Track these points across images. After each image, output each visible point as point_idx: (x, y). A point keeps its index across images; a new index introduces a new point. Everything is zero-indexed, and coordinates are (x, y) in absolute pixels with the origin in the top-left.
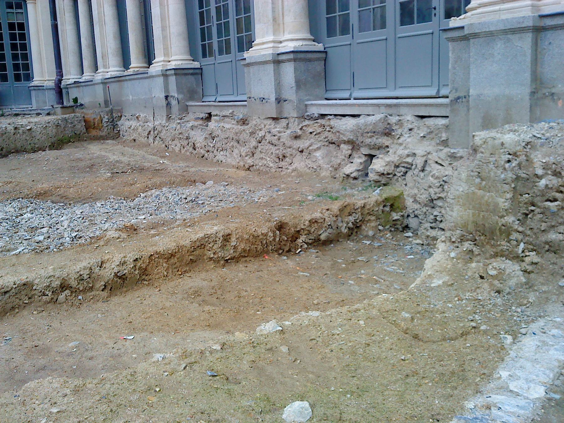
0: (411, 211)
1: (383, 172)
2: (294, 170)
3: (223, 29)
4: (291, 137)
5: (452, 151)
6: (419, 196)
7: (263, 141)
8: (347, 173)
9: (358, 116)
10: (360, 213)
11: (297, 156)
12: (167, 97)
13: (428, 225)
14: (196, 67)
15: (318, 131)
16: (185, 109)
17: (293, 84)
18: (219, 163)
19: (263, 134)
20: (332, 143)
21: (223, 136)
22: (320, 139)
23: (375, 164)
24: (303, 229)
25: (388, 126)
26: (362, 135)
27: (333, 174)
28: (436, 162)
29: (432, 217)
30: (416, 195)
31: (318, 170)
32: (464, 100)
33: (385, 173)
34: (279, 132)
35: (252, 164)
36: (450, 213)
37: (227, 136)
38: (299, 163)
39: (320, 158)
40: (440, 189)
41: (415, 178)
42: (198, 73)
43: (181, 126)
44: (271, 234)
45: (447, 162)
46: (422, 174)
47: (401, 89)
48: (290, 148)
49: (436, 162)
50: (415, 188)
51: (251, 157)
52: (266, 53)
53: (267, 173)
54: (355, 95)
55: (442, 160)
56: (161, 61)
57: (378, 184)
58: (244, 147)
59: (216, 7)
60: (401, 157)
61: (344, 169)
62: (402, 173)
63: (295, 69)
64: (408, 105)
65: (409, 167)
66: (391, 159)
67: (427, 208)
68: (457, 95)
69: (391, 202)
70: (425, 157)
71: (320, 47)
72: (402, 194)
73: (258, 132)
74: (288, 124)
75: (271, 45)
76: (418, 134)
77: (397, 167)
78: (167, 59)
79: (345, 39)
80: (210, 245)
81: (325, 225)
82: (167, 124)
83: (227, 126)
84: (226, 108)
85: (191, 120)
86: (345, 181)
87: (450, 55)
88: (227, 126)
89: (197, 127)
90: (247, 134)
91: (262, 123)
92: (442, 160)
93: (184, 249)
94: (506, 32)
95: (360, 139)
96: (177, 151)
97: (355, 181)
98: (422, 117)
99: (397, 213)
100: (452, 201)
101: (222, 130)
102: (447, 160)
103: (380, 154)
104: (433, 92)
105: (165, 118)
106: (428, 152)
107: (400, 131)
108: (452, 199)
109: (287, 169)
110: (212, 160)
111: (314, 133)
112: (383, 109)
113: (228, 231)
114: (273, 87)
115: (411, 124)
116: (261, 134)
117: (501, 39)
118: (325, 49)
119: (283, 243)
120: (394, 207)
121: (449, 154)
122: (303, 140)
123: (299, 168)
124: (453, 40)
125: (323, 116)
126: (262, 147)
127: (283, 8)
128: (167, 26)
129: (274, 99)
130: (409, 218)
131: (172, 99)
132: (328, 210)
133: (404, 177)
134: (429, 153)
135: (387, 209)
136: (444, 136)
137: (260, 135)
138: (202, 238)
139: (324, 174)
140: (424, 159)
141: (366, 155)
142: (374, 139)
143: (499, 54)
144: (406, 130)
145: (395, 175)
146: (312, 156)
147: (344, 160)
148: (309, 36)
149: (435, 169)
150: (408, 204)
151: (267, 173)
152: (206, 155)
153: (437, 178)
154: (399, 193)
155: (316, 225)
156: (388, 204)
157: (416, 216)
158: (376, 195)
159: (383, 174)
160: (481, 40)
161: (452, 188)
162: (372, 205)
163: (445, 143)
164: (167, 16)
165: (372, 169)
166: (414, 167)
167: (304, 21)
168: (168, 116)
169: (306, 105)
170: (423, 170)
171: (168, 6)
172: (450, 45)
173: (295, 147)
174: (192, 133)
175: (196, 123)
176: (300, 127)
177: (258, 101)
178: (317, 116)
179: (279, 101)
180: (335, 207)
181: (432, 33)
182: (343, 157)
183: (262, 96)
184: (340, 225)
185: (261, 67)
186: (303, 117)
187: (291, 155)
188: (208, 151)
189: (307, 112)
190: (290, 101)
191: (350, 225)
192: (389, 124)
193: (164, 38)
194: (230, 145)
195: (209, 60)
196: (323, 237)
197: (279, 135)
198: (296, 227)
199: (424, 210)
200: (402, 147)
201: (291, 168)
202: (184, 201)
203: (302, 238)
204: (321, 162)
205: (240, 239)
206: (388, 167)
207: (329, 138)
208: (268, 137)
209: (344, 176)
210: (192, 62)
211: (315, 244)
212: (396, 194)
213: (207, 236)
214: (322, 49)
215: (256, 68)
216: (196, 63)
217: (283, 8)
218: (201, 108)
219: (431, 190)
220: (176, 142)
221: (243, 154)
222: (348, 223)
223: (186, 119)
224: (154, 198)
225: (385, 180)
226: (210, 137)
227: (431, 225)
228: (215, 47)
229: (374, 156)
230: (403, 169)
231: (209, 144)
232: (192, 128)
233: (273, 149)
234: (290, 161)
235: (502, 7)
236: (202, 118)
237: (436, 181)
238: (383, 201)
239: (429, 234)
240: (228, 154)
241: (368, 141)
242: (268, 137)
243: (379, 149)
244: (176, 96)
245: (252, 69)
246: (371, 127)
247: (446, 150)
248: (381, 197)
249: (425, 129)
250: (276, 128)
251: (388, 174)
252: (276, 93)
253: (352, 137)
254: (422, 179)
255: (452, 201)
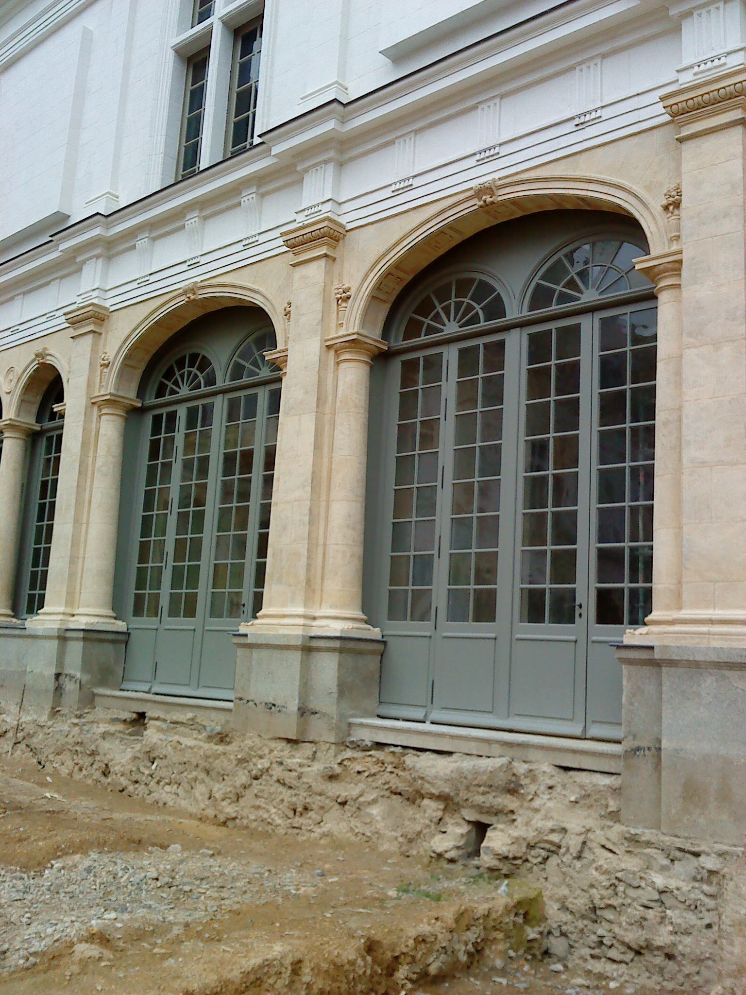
0: (555, 926)
1: (506, 854)
2: (324, 835)
3: (186, 577)
4: (323, 777)
5: (633, 831)
6: (570, 900)
7: (264, 777)
8: (439, 850)
9: (450, 753)
10: (482, 927)
11: (333, 811)
12: (58, 676)
13: (586, 952)
14: (120, 630)
15: (373, 771)
16: (89, 700)
17: (335, 689)
18: (160, 806)
19: (267, 765)
20: (396, 794)
21: (176, 758)
22: (374, 785)
23: (490, 839)
24: (404, 954)
25: (514, 779)
26: (468, 788)
27: (404, 848)
28: (603, 846)
29: (594, 938)
30: (565, 897)
31: (374, 840)
32: (647, 752)
33: (511, 856)
34: (301, 765)
35: (234, 815)
36: (729, 948)
37: (185, 760)
38: (336, 824)
39: (379, 818)
40: (610, 891)
41: (564, 869)
42: (123, 639)
43: (81, 730)
44: (360, 962)
45: (623, 848)
46: (578, 864)
47: (517, 718)
48: (321, 794)
49: (603, 846)
50: (563, 887)
51: (233, 802)
52: (290, 633)
53: (267, 835)
54: (436, 715)
55: (614, 843)
56: (59, 614)
57: (496, 873)
58: (218, 782)
59: (176, 540)
60: (540, 832)
61: (432, 843)
62: (540, 859)
63: (340, 665)
64: (542, 748)
65: (555, 849)
66: (521, 833)
67: (585, 922)
68: (637, 744)
69: (526, 909)
70: (583, 836)
71: (375, 633)
72: (540, 895)
73: (254, 760)
74: (315, 752)
75: (301, 621)
76: (564, 795)
77: (531, 847)
78: (69, 611)
79: (423, 628)
80: (271, 981)
81: (437, 947)
82: (50, 723)
83: (187, 742)
84: (180, 708)
85: (102, 722)
86: (434, 865)
87: (624, 683)
88: (187, 742)
89: (113, 735)
90: (230, 760)
91: (266, 745)
92: (614, 843)
93: (230, 986)
94: (719, 665)
95: (463, 795)
96: (63, 775)
97: (451, 866)
98: (567, 769)
99: (532, 927)
100: (730, 930)
101: (175, 748)
102: (622, 844)
103: (498, 822)
104: (577, 731)
105: (47, 711)
106: (588, 827)
107: (532, 788)
108: (730, 926)
109: (311, 831)
110: (144, 799)
111: (366, 774)
112: (496, 749)
113: (298, 956)
114: (297, 688)
115: (550, 778)
116: (262, 764)
117: (711, 674)
118: (383, 636)
119: (376, 978)
120: (529, 917)
121: (628, 835)
122: (343, 783)
123: (336, 833)
124: (630, 662)
125: (379, 746)
126: (261, 787)
127: (323, 568)
128: (81, 555)
129: (296, 709)
130: (551, 937)
131: (67, 680)
132: (437, 919)
133: (543, 866)
134: (589, 831)
135: (520, 920)
136: (613, 805)
137: (260, 767)
138: (261, 967)
139: (385, 847)
140: (581, 839)
141: (469, 822)
142: (490, 797)
143: (709, 694)
144: (542, 788)
145: (527, 860)
146: (362, 813)
147: (428, 826)
148: (359, 614)
149: (604, 858)
150: (550, 912)
151: (267, 835)
152: (131, 788)
153: (606, 872)
154: (536, 893)
155: (423, 946)
156: (522, 911)
157: (563, 934)
158: (502, 896)
159: (506, 858)
160: (680, 670)
161: (727, 908)
162: (500, 913)
163: (615, 816)
164: (82, 539)
165: (488, 848)
166: (563, 850)
167: (355, 590)
168: (53, 708)
169: (350, 725)
170: (579, 857)
171: (88, 524)
172: (625, 669)
173: (330, 794)
174: (105, 745)
175: (112, 728)
176: (339, 761)
177: (261, 708)
178: (369, 744)
179: (304, 712)
180: (449, 914)
181: (576, 641)
182: (427, 822)
183: (271, 700)
184: (457, 947)
185: (277, 654)
186: (343, 745)
187: (322, 808)
188: (136, 782)
189: (349, 735)
190: (324, 715)
191: (470, 947)
192: (514, 775)
193: (72, 575)
194: (190, 776)
195: (146, 622)
196: (433, 970)
197: (299, 769)
198: (393, 950)
199: (580, 924)
200: (539, 816)
201: (318, 830)
202: (154, 884)
203: (402, 973)
204: (380, 825)
205: (316, 970)
206: (515, 847)
207: (391, 785)
208: (277, 772)
209: (433, 855)
210: (114, 621)
211: (422, 982)
212: (532, 894)
213: (267, 963)
214: (379, 638)
215: (265, 653)
216: (120, 623)
217: (323, 568)
218: (120, 703)
219: (593, 891)
220: (66, 756)
221: (218, 795)
222: (466, 944)
223: (89, 718)
224: (85, 874)
225: (509, 867)
226: (146, 756)
227: (593, 952)
228: (164, 602)
229: (489, 825)
230: (544, 853)
231: (142, 769)
232: (104, 736)
233: (286, 794)
234: (319, 819)
235: (711, 629)
236: (125, 720)
237: (602, 878)
238: (514, 907)
239: (589, 967)
240: (180, 791)
241: (479, 799)
242: (277, 772)
243: (496, 814)
244: (78, 675)
245: (256, 653)
246: (485, 778)
247: (618, 828)
248: (512, 898)
249: (577, 789)
250: (296, 758)
251: (515, 858)
252: (300, 699)
253: (447, 790)
254: (579, 872)
255: (730, 930)
